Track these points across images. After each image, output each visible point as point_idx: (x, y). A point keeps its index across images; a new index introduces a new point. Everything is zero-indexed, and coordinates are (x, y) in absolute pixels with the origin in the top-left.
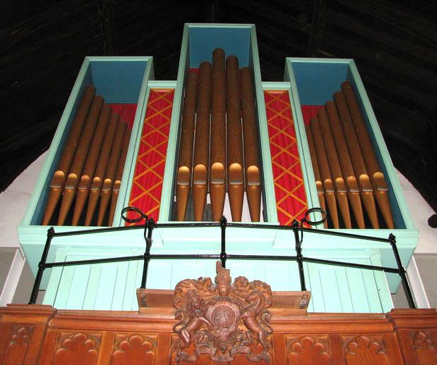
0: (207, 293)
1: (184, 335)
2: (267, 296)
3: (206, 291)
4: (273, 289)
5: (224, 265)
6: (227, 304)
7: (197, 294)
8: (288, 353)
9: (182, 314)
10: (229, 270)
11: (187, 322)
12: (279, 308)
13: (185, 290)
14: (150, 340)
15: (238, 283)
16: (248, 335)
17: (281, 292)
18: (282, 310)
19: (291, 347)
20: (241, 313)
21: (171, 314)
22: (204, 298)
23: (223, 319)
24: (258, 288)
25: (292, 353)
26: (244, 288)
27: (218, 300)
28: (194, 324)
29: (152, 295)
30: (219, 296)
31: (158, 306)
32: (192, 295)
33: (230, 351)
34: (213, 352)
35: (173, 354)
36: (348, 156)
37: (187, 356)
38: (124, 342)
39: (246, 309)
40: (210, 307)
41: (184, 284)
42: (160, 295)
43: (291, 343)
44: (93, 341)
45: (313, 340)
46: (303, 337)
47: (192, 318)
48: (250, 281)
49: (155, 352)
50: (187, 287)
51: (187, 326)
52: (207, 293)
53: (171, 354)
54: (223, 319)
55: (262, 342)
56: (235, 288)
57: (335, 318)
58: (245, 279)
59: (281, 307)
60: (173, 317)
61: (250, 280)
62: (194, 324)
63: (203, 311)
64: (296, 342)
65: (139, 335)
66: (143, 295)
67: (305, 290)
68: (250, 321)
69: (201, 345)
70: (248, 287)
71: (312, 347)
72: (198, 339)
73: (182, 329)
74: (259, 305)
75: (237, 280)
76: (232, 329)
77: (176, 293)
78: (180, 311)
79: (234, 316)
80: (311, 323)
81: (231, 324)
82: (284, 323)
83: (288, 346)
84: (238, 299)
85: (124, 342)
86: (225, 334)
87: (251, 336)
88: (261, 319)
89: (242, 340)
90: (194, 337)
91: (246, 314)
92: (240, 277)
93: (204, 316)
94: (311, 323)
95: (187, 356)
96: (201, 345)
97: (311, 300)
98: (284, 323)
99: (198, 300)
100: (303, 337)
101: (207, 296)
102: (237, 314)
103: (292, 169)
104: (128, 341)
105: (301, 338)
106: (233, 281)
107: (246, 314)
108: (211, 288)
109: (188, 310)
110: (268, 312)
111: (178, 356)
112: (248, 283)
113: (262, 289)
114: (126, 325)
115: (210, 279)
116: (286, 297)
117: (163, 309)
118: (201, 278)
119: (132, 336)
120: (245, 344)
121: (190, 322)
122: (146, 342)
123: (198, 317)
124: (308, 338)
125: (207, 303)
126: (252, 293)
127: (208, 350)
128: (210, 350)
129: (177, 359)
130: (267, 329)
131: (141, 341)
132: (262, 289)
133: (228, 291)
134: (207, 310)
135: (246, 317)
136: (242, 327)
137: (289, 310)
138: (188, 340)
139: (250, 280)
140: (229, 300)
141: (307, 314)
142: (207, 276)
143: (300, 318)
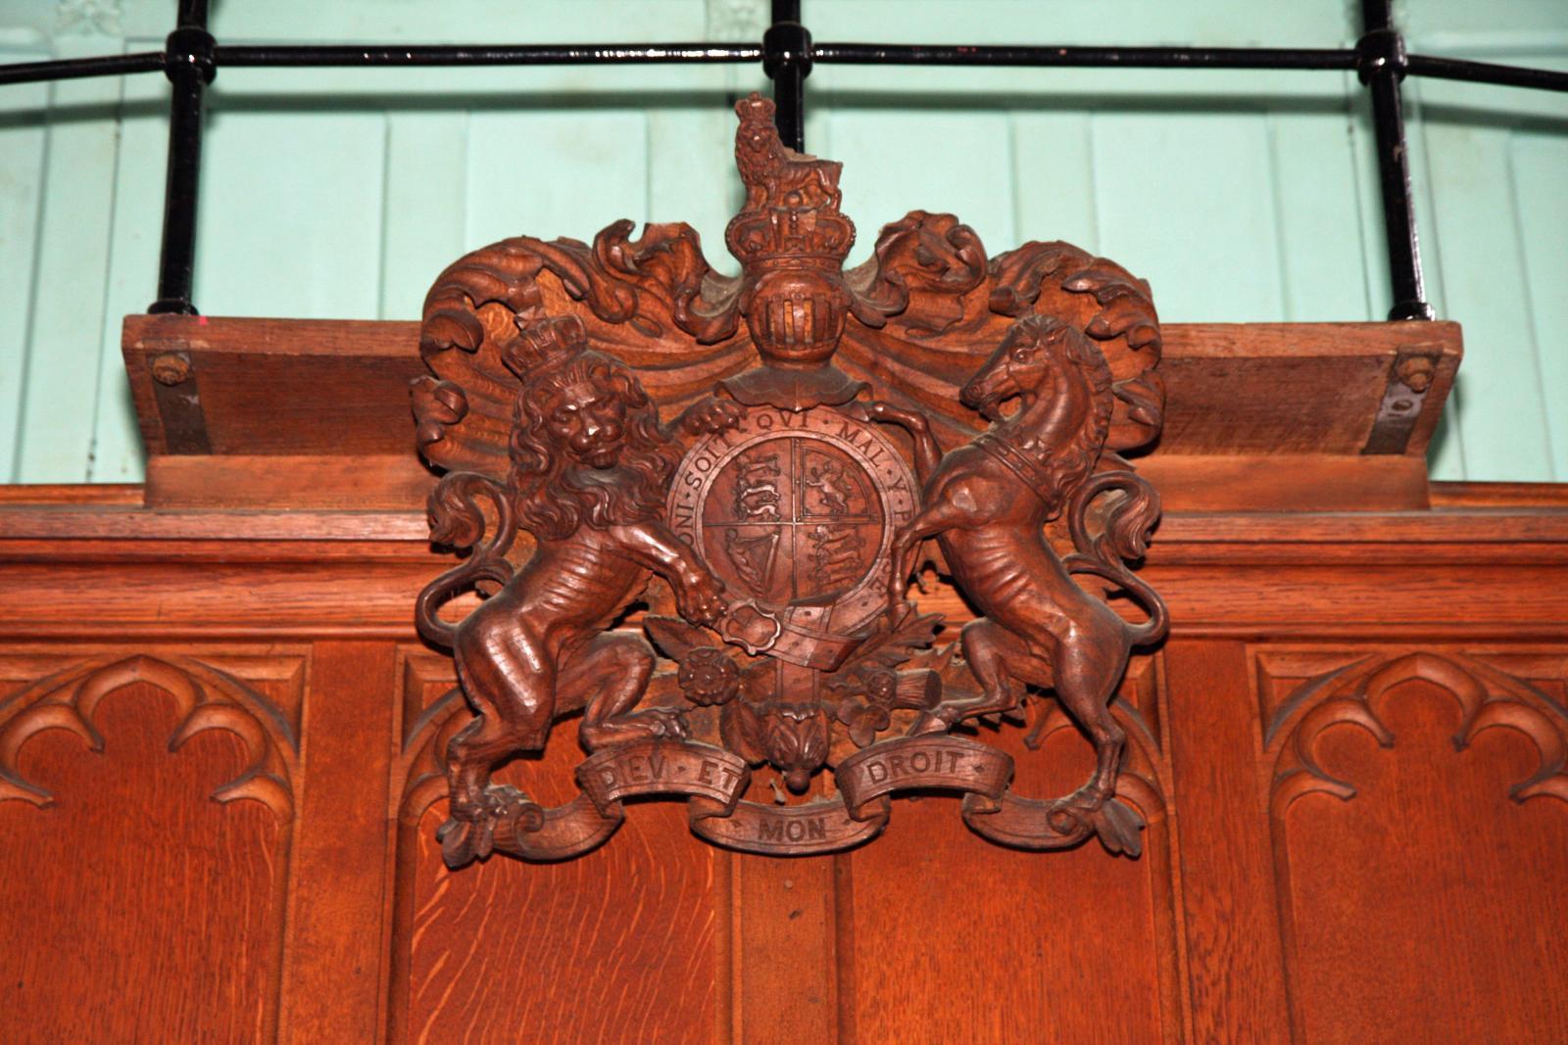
0: (667, 345)
1: (503, 664)
2: (1124, 366)
3: (656, 331)
4: (1170, 309)
5: (791, 130)
6: (824, 427)
7: (596, 348)
8: (1281, 782)
9: (483, 504)
10: (834, 169)
11: (519, 560)
12: (1207, 449)
13: (497, 322)
14: (243, 698)
15: (897, 267)
16: (983, 653)
17: (1228, 331)
18: (1230, 461)
19: (1297, 736)
20: (930, 492)
21: (399, 500)
22: (648, 380)
23: (795, 541)
24: (1061, 300)
25: (1309, 784)
26: (945, 305)
27: (750, 400)
28: (570, 583)
29: (240, 358)
30: (757, 365)
31: (301, 449)
32: (556, 357)
33: (844, 783)
34: (722, 787)
35: (427, 797)
36: (659, 295)
37: (531, 817)
38: (40, 721)
39: (969, 465)
40: (696, 448)
41: (498, 275)
42: (309, 360)
43: (1296, 713)
44: (242, 727)
45: (1463, 691)
46: (1387, 666)
47: (556, 536)
48: (993, 249)
49: (285, 788)
50: (511, 305)
51: (519, 591)
52: (667, 345)
53: (408, 797)
54: (795, 541)
55: (1087, 706)
56: (877, 307)
57: (1209, 574)
58: (958, 235)
59: (1223, 442)
60: (414, 527)
61: (996, 243)
62: (570, 583)
63: (640, 477)
64: (1332, 700)
65: (154, 662)
66: (169, 366)
67: (1418, 310)
68: (996, 551)
69: (626, 733)
70: (980, 297)
71: (1461, 745)
72: (606, 684)
73: (479, 618)
74: (1067, 430)
75: (900, 237)
76: (860, 609)
77: (429, 349)
78: (471, 485)
79: (874, 513)
80: (1454, 564)
81: (856, 572)
82: (1241, 563)
83: (1280, 735)
84: (900, 385)
85: (40, 721)
86: (809, 647)
87: (1000, 662)
88: (1076, 536)
89: (933, 689)
90: (577, 674)
91: (963, 500)
92: (920, 219)
93: (652, 518)
94: (1454, 564)
95: (531, 817)
96: (626, 733)
97: (436, 654)
98: (1241, 563)
99: (604, 397)
100: (1387, 666)
101: (671, 362)
102: (896, 502)
103: (789, 19)
104: (75, 709)
105: (1371, 677)
106: (861, 254)
107: (963, 500)
108: (700, 311)
109: (528, 472)
110: (1130, 487)
111: (458, 813)
112: (979, 267)
113: (1089, 315)
114: (58, 594)
115: (686, 236)
116: (1263, 365)
117: (338, 463)
118: (621, 229)
119: (98, 673)
120: (956, 727)
121: (545, 562)
122: (219, 719)
123: (604, 524)
124: (1428, 672)
125: (667, 415)
126: (1009, 347)
127: (684, 772)
128: (694, 765)
129: (456, 837)
130: (1122, 612)
131: (169, 702)
132: (1089, 315)
133: (827, 326)
134: (671, 471)
135: (968, 525)
136: (939, 601)
137: (1284, 466)
138: (530, 702)
139: (996, 243)
140: (842, 403)
141: (1423, 492)
142: (665, 216)
143: (1375, 523)
